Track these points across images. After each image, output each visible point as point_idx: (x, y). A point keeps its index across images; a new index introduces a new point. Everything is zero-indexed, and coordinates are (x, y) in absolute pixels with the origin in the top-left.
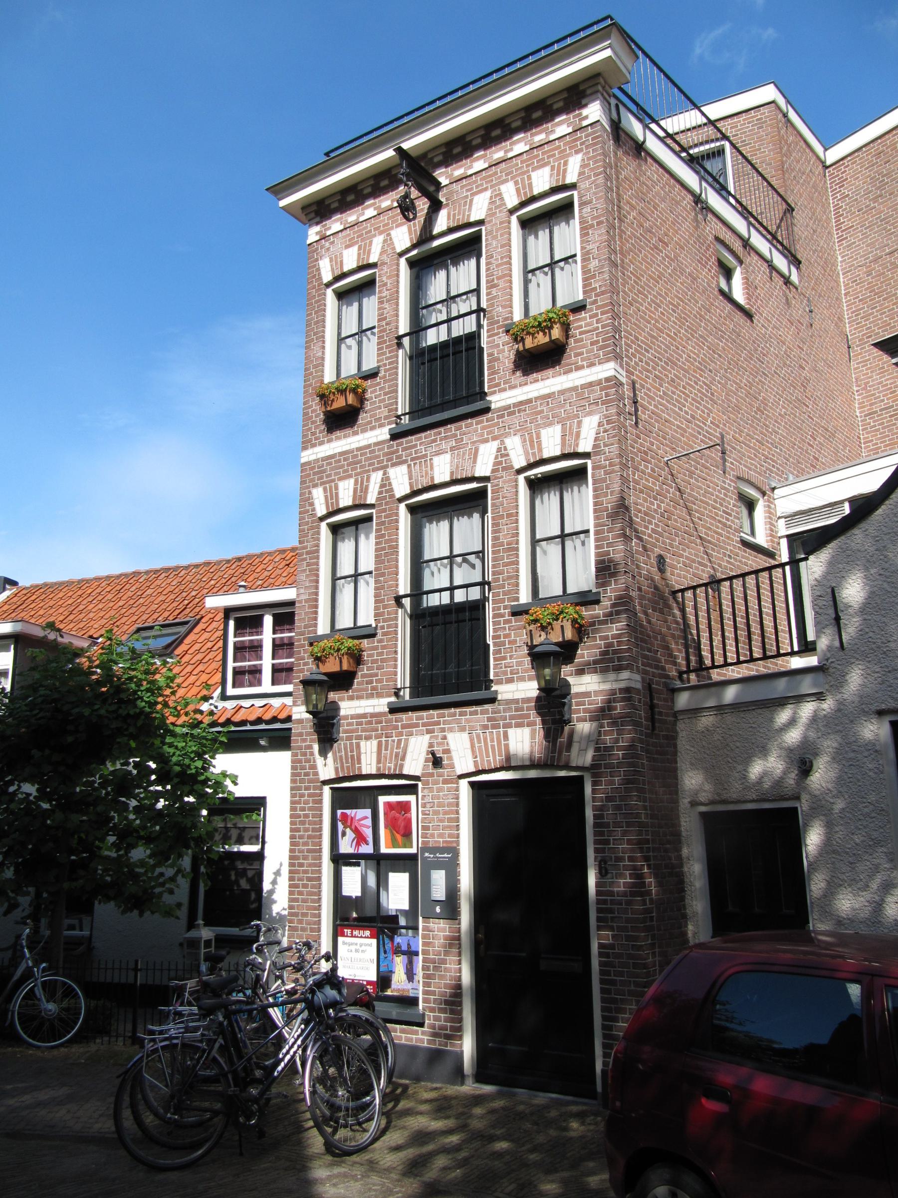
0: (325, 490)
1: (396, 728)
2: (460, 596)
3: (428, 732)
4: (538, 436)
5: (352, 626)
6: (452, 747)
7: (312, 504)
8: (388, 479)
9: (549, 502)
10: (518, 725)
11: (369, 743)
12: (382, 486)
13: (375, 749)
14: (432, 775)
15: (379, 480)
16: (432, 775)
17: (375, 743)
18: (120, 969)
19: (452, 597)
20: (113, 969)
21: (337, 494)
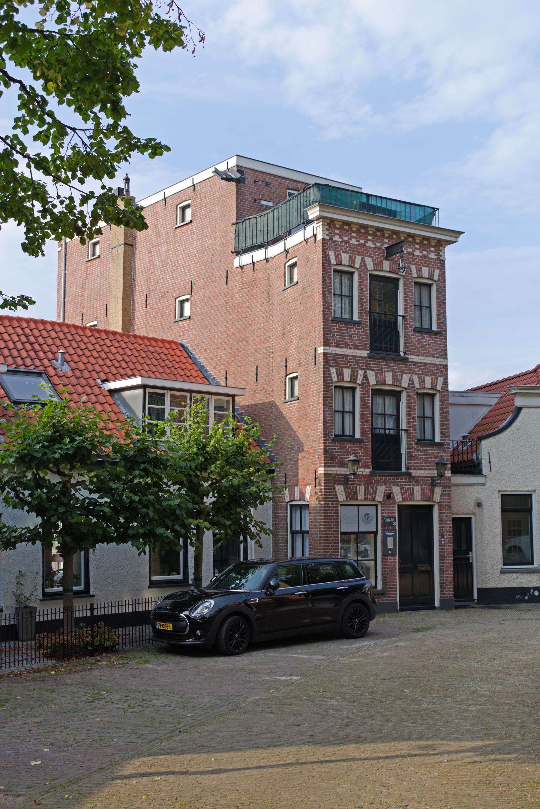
0: (352, 371)
1: (372, 482)
2: (387, 432)
3: (385, 485)
4: (424, 378)
5: (342, 434)
6: (394, 491)
7: (330, 374)
8: (366, 375)
9: (379, 400)
10: (417, 485)
11: (361, 487)
12: (364, 377)
13: (363, 489)
14: (386, 502)
15: (362, 374)
16: (386, 502)
17: (363, 487)
18: (129, 605)
19: (385, 431)
20: (152, 602)
21: (437, 382)
